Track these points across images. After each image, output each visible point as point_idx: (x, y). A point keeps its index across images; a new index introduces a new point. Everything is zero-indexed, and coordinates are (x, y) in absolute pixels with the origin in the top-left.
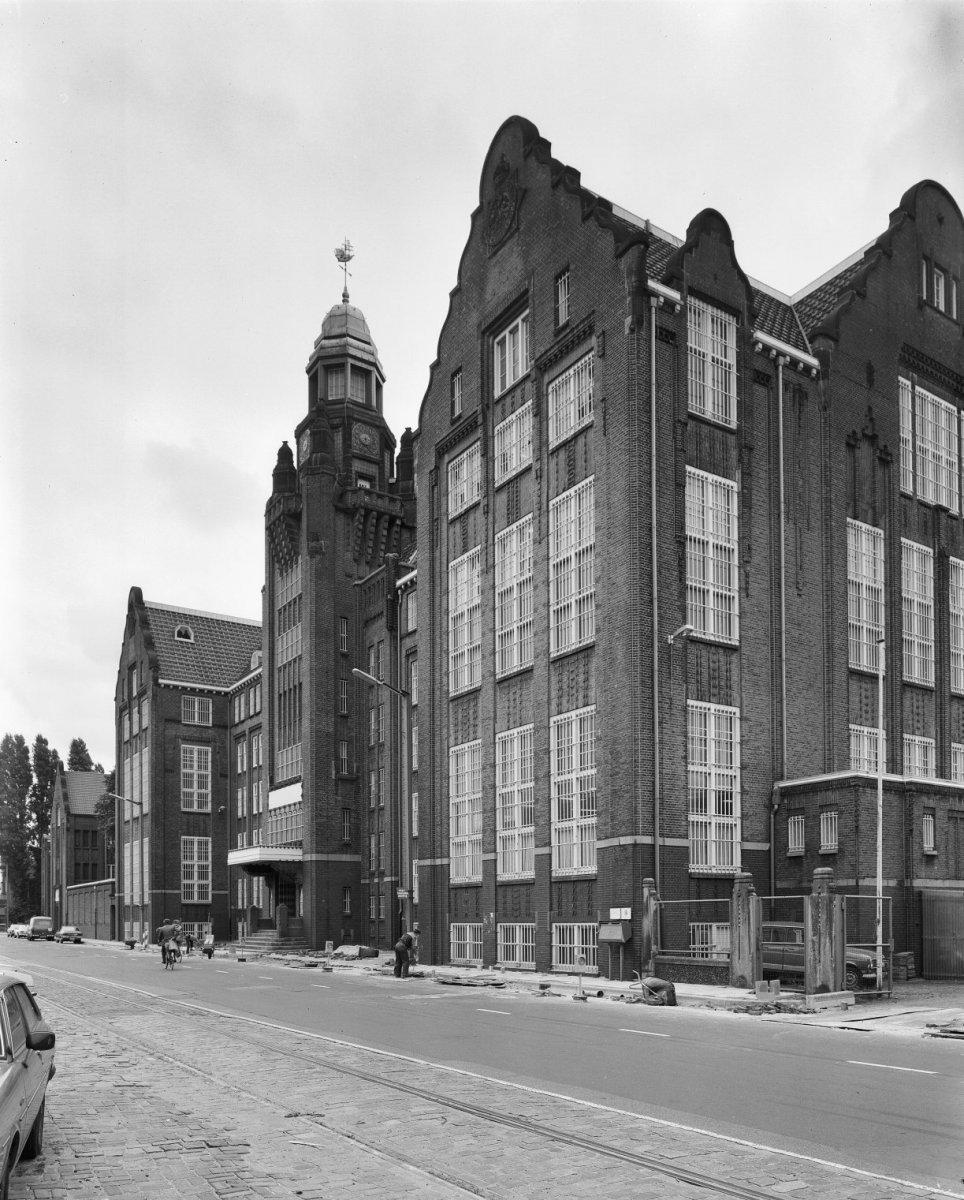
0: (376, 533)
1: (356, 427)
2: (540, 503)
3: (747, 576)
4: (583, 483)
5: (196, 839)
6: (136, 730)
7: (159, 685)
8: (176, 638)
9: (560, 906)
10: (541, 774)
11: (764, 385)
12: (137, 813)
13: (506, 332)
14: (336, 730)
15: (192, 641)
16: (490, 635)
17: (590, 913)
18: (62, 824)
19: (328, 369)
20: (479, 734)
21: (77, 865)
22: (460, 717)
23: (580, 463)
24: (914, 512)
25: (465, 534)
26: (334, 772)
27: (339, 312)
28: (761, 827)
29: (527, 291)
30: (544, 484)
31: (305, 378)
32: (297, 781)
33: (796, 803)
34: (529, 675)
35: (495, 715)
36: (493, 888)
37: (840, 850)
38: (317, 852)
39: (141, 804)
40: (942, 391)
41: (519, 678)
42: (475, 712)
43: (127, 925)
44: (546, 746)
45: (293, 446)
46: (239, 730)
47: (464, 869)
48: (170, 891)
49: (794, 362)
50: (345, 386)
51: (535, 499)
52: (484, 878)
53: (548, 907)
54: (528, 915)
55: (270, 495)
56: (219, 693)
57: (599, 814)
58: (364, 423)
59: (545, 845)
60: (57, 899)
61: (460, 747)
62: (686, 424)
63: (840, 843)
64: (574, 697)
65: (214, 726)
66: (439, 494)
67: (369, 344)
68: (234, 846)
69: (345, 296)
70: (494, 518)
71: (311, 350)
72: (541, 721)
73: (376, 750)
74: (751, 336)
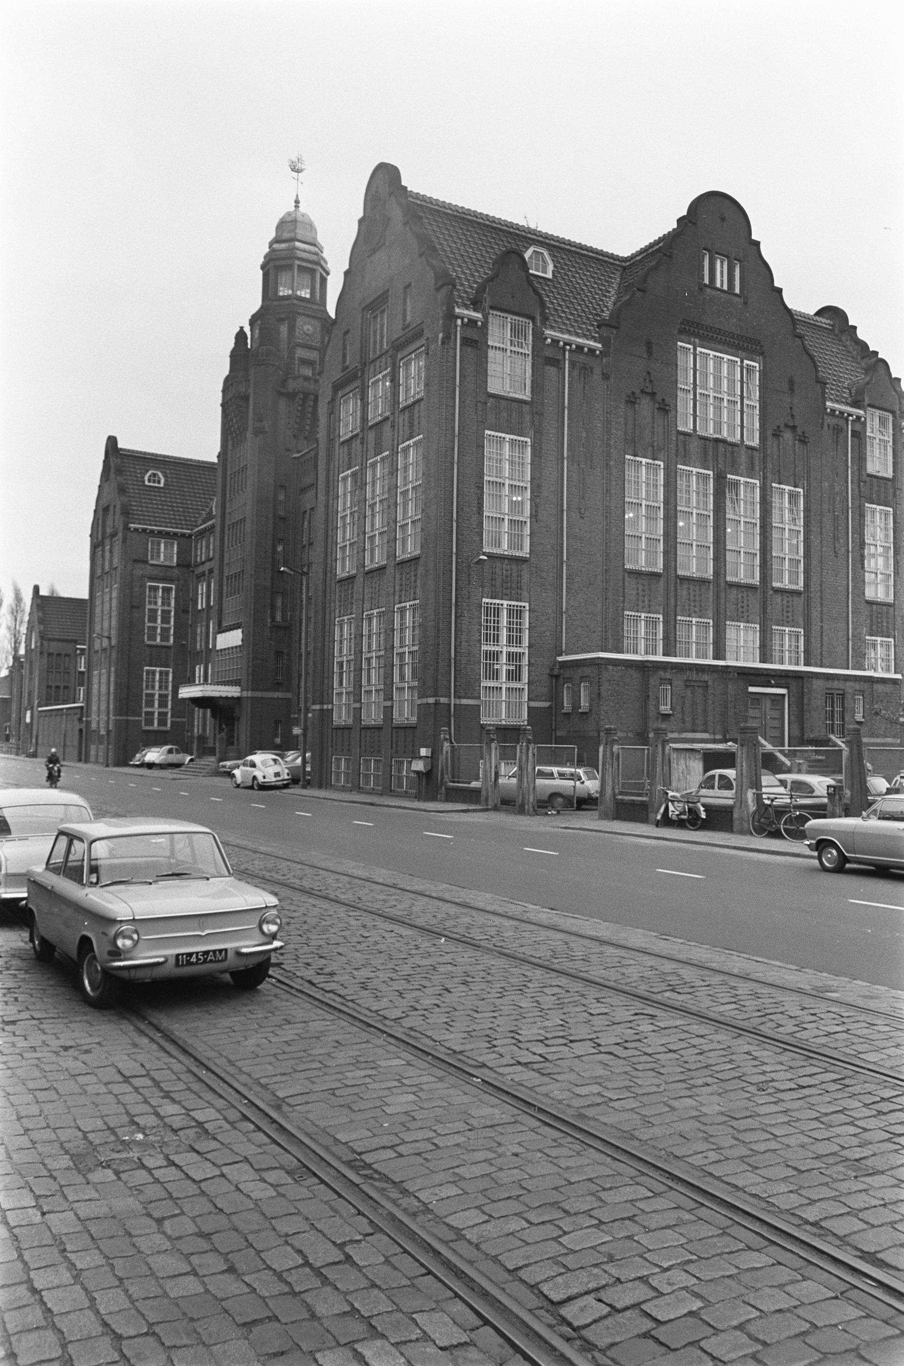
1: (300, 321)
2: (393, 445)
3: (536, 507)
5: (158, 669)
6: (107, 568)
7: (129, 529)
8: (147, 483)
9: (397, 746)
12: (105, 643)
13: (378, 312)
15: (162, 485)
16: (362, 536)
17: (379, 751)
18: (36, 647)
19: (279, 269)
21: (49, 687)
27: (289, 219)
28: (545, 690)
29: (388, 291)
30: (396, 431)
31: (261, 272)
32: (239, 628)
33: (567, 673)
36: (358, 729)
37: (591, 710)
38: (253, 690)
39: (109, 638)
40: (727, 349)
42: (352, 593)
43: (93, 748)
45: (247, 330)
46: (200, 570)
47: (341, 717)
48: (132, 718)
49: (580, 348)
56: (183, 535)
58: (308, 316)
60: (28, 720)
62: (486, 403)
63: (591, 705)
65: (178, 565)
67: (314, 245)
68: (190, 681)
69: (297, 202)
71: (267, 250)
74: (543, 334)
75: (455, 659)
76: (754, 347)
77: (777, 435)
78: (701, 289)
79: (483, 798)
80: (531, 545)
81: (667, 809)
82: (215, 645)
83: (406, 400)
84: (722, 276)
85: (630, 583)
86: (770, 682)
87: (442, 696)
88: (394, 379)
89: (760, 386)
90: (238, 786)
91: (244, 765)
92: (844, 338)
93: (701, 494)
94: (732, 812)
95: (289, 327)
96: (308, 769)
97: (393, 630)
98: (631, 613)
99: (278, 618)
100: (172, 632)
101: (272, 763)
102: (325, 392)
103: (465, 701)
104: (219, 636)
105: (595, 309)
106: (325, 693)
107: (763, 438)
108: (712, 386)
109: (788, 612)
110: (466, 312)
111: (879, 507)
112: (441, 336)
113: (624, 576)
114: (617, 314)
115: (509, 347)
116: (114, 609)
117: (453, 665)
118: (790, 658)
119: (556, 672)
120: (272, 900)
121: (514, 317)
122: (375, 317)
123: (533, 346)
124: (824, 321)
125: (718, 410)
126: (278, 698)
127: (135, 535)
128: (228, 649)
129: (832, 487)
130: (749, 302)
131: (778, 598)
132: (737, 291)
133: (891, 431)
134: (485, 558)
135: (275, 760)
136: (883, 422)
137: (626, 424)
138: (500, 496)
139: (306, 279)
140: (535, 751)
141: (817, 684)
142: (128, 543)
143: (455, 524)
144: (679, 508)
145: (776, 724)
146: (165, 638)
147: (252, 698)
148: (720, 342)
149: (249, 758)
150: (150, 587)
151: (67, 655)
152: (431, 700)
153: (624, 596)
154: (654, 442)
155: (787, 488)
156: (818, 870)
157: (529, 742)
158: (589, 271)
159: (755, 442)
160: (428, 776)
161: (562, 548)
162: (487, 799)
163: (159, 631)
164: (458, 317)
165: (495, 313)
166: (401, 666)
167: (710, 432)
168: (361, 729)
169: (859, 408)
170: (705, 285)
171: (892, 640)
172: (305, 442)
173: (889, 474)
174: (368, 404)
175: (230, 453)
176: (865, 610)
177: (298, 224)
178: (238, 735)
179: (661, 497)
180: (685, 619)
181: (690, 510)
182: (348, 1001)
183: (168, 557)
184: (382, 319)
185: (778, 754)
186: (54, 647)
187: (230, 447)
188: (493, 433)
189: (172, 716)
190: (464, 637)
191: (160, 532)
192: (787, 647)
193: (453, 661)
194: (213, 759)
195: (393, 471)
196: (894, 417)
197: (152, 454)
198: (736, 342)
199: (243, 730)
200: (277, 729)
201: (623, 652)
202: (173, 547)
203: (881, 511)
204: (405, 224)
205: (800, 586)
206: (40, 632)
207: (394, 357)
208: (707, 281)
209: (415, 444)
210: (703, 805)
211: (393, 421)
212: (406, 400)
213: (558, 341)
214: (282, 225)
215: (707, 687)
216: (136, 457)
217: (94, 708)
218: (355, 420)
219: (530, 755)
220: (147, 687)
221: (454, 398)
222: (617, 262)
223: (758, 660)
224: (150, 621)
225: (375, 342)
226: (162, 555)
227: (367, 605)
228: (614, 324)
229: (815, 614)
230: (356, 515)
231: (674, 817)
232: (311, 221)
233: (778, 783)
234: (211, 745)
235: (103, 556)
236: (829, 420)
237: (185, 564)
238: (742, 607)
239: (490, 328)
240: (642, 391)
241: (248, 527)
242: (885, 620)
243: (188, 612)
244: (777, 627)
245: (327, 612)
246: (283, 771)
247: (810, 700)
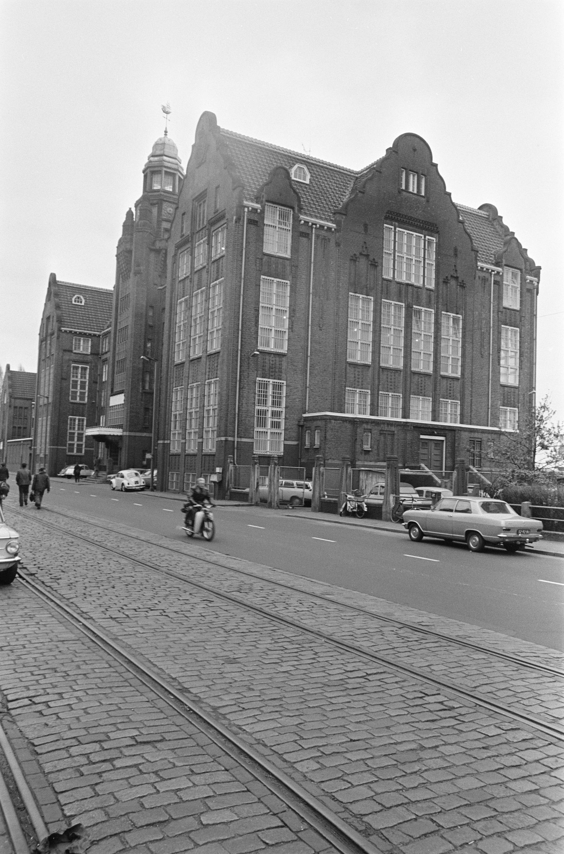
1: (165, 205)
5: (77, 417)
7: (61, 331)
8: (73, 303)
9: (204, 466)
11: (306, 237)
12: (46, 402)
13: (202, 202)
14: (144, 366)
15: (83, 304)
17: (195, 469)
18: (7, 402)
19: (153, 173)
21: (14, 427)
24: (393, 288)
28: (294, 434)
31: (142, 175)
32: (123, 393)
33: (308, 424)
34: (199, 360)
37: (320, 447)
39: (48, 398)
40: (416, 229)
46: (104, 357)
49: (322, 227)
50: (162, 178)
56: (95, 335)
62: (262, 259)
63: (321, 444)
65: (91, 354)
67: (175, 159)
69: (166, 132)
75: (238, 414)
76: (433, 228)
77: (446, 282)
78: (399, 192)
79: (249, 498)
80: (288, 346)
81: (346, 505)
83: (215, 256)
84: (413, 184)
85: (350, 370)
86: (434, 432)
87: (230, 436)
88: (209, 243)
89: (436, 252)
90: (114, 489)
91: (117, 476)
92: (495, 223)
93: (397, 317)
94: (381, 508)
95: (158, 209)
97: (204, 396)
98: (350, 389)
100: (87, 395)
101: (134, 475)
102: (171, 251)
103: (244, 440)
105: (335, 203)
107: (437, 284)
108: (405, 251)
109: (450, 390)
110: (251, 204)
111: (510, 328)
112: (235, 218)
113: (346, 366)
114: (346, 205)
115: (277, 226)
116: (51, 380)
118: (451, 418)
119: (302, 423)
120: (14, 534)
121: (281, 207)
122: (200, 205)
123: (293, 225)
124: (483, 213)
125: (409, 266)
127: (64, 334)
128: (116, 406)
129: (480, 315)
130: (431, 200)
131: (444, 382)
132: (423, 194)
133: (519, 282)
134: (258, 353)
135: (136, 474)
136: (514, 275)
137: (350, 274)
138: (270, 316)
139: (170, 179)
140: (279, 470)
141: (465, 435)
142: (60, 339)
143: (240, 332)
144: (382, 325)
145: (438, 458)
146: (82, 398)
147: (129, 436)
148: (411, 225)
149: (121, 472)
150: (74, 367)
151: (26, 408)
153: (346, 378)
154: (367, 285)
155: (452, 315)
156: (408, 540)
157: (275, 464)
158: (333, 179)
159: (432, 286)
160: (220, 484)
161: (307, 348)
162: (252, 499)
163: (78, 394)
164: (245, 207)
165: (269, 204)
166: (208, 417)
167: (404, 280)
168: (185, 455)
169: (499, 266)
170: (402, 190)
171: (516, 409)
173: (518, 307)
175: (121, 286)
176: (500, 390)
177: (166, 146)
178: (120, 458)
179: (371, 319)
180: (385, 393)
181: (389, 327)
182: (47, 586)
183: (85, 348)
184: (204, 207)
185: (434, 476)
186: (18, 403)
187: (121, 282)
188: (266, 277)
189: (86, 447)
191: (80, 333)
192: (449, 412)
193: (237, 415)
194: (104, 473)
195: (207, 299)
196: (521, 272)
197: (78, 285)
198: (422, 225)
199: (123, 456)
201: (344, 412)
202: (88, 342)
203: (512, 330)
204: (218, 149)
205: (459, 375)
206: (10, 393)
207: (209, 230)
208: (403, 187)
209: (220, 283)
210: (366, 504)
211: (208, 269)
212: (215, 256)
213: (308, 223)
214: (156, 145)
215: (394, 434)
216: (68, 286)
217: (39, 441)
218: (187, 267)
219: (276, 472)
220: (70, 428)
221: (242, 256)
222: (352, 174)
223: (401, 417)
224: (73, 388)
225: (200, 220)
226: (81, 348)
227: (190, 381)
228: (343, 212)
229: (467, 392)
231: (350, 511)
232: (174, 144)
233: (415, 492)
235: (46, 347)
236: (479, 274)
237: (96, 353)
238: (421, 387)
239: (266, 213)
240: (361, 254)
242: (512, 397)
244: (443, 400)
245: (169, 383)
246: (141, 481)
247: (459, 444)
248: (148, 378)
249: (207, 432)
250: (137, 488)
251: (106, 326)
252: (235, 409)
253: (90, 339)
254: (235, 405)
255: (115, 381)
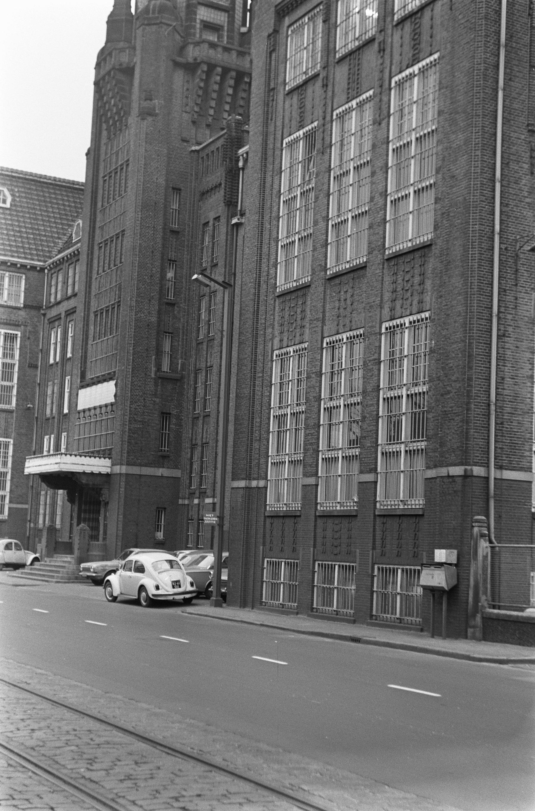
0: (220, 92)
2: (381, 79)
4: (428, 61)
9: (383, 546)
10: (312, 395)
15: (8, 205)
16: (322, 224)
20: (306, 337)
22: (287, 316)
23: (425, 37)
25: (302, 106)
26: (154, 369)
32: (111, 379)
34: (361, 272)
35: (324, 316)
38: (128, 464)
41: (352, 275)
44: (376, 357)
46: (53, 312)
51: (377, 75)
52: (303, 507)
53: (370, 545)
54: (349, 553)
55: (103, 45)
56: (33, 268)
57: (428, 439)
59: (370, 471)
61: (284, 351)
64: (409, 301)
65: (26, 306)
66: (277, 61)
68: (38, 452)
70: (333, 92)
72: (372, 327)
73: (205, 344)
82: (73, 403)
90: (114, 599)
96: (224, 577)
99: (165, 367)
101: (167, 566)
104: (82, 392)
106: (254, 463)
117: (493, 412)
126: (162, 476)
147: (127, 475)
152: (457, 471)
172: (208, 132)
174: (336, 27)
175: (103, 148)
178: (105, 526)
187: (104, 140)
189: (10, 502)
190: (507, 370)
194: (68, 558)
200: (159, 519)
202: (19, 283)
209: (423, 71)
230: (312, 195)
234: (66, 540)
241: (128, 242)
243: (36, 367)
245: (260, 340)
246: (185, 579)
248: (167, 347)
249: (330, 461)
250: (177, 597)
251: (56, 250)
252: (488, 391)
253: (24, 277)
254: (489, 379)
255: (89, 354)
